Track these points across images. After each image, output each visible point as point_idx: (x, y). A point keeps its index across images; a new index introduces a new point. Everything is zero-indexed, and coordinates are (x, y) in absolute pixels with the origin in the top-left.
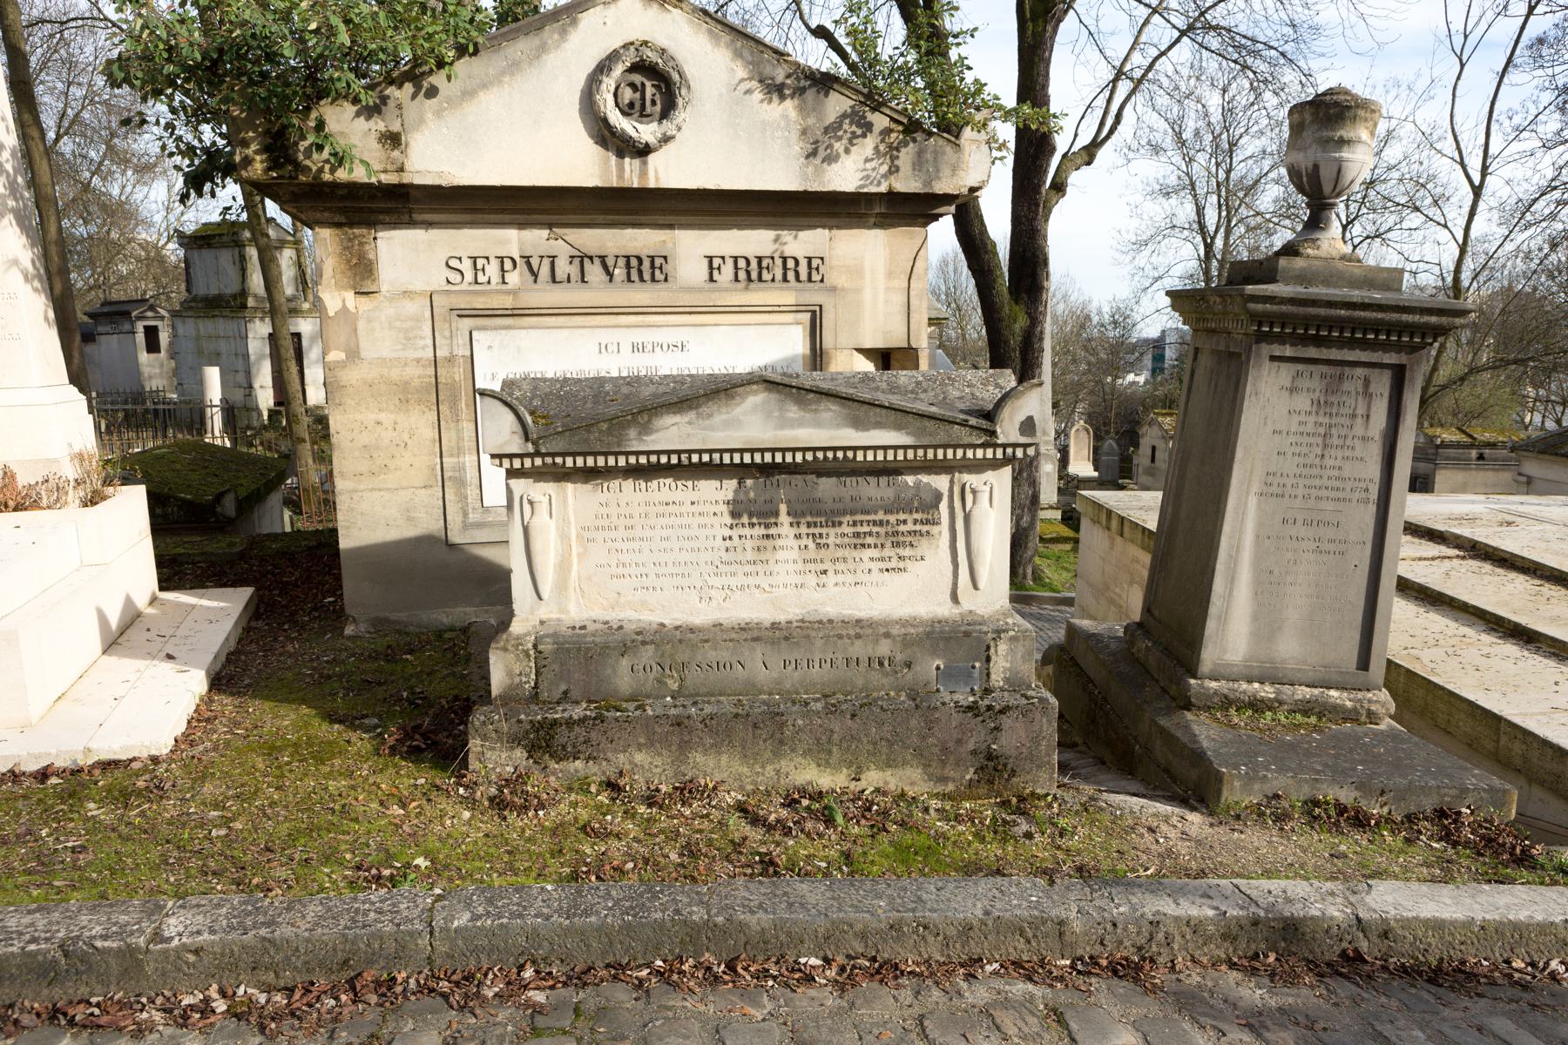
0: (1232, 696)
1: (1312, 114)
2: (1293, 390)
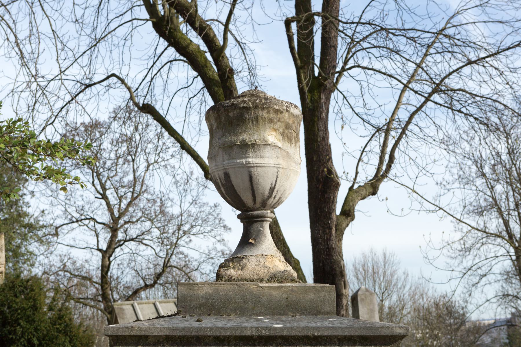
1: (216, 119)
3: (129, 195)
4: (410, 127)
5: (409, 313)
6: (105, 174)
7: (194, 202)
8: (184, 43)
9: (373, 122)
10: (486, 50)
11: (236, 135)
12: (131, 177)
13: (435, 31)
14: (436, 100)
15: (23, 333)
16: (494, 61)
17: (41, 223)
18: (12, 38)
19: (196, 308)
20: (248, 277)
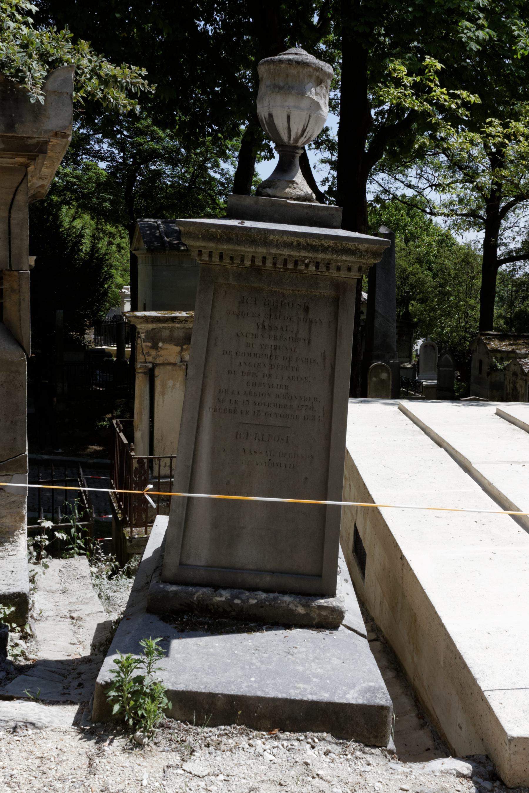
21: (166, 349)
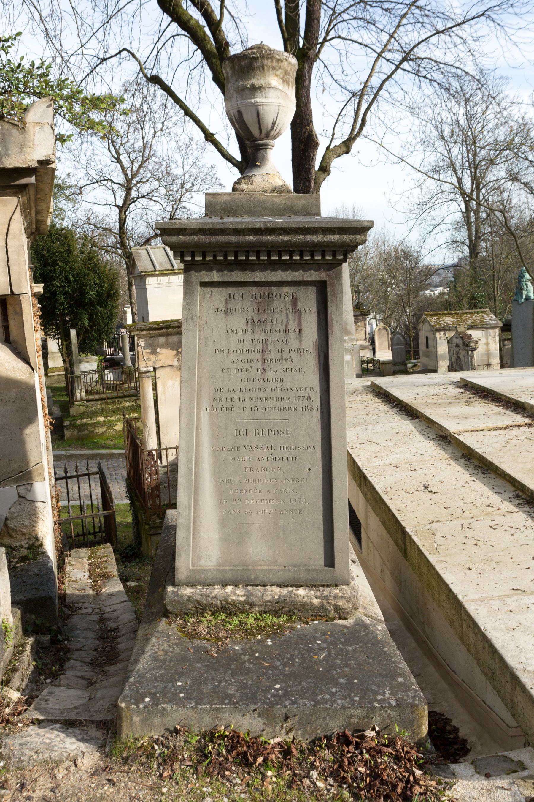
0: (205, 602)
1: (231, 68)
2: (227, 312)
3: (140, 159)
4: (381, 93)
5: (372, 258)
6: (119, 141)
7: (194, 164)
8: (186, 19)
9: (349, 88)
10: (453, 20)
11: (247, 80)
12: (140, 143)
13: (408, 2)
14: (405, 68)
15: (61, 272)
16: (459, 31)
17: (68, 184)
18: (37, 17)
19: (218, 211)
20: (256, 190)
21: (162, 354)
